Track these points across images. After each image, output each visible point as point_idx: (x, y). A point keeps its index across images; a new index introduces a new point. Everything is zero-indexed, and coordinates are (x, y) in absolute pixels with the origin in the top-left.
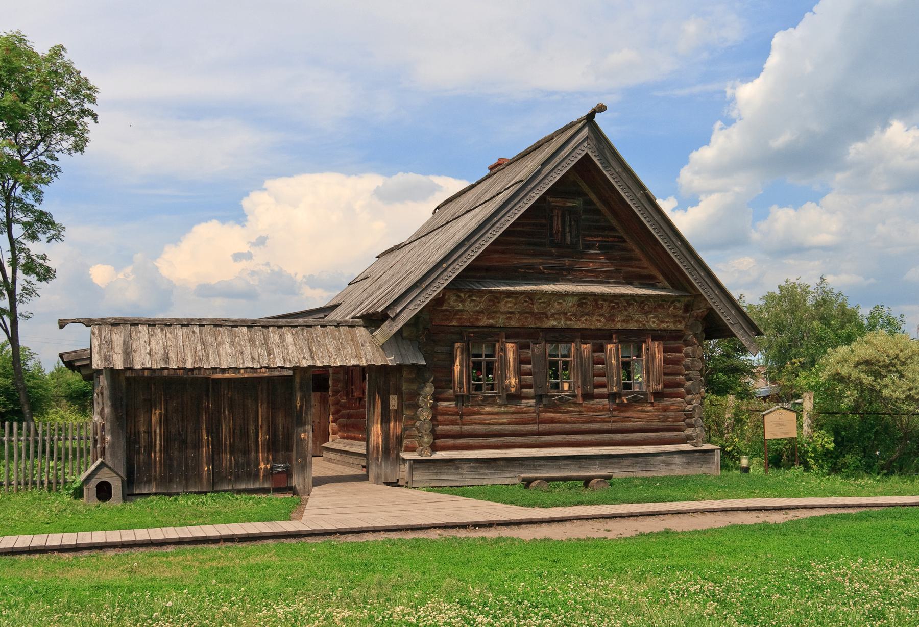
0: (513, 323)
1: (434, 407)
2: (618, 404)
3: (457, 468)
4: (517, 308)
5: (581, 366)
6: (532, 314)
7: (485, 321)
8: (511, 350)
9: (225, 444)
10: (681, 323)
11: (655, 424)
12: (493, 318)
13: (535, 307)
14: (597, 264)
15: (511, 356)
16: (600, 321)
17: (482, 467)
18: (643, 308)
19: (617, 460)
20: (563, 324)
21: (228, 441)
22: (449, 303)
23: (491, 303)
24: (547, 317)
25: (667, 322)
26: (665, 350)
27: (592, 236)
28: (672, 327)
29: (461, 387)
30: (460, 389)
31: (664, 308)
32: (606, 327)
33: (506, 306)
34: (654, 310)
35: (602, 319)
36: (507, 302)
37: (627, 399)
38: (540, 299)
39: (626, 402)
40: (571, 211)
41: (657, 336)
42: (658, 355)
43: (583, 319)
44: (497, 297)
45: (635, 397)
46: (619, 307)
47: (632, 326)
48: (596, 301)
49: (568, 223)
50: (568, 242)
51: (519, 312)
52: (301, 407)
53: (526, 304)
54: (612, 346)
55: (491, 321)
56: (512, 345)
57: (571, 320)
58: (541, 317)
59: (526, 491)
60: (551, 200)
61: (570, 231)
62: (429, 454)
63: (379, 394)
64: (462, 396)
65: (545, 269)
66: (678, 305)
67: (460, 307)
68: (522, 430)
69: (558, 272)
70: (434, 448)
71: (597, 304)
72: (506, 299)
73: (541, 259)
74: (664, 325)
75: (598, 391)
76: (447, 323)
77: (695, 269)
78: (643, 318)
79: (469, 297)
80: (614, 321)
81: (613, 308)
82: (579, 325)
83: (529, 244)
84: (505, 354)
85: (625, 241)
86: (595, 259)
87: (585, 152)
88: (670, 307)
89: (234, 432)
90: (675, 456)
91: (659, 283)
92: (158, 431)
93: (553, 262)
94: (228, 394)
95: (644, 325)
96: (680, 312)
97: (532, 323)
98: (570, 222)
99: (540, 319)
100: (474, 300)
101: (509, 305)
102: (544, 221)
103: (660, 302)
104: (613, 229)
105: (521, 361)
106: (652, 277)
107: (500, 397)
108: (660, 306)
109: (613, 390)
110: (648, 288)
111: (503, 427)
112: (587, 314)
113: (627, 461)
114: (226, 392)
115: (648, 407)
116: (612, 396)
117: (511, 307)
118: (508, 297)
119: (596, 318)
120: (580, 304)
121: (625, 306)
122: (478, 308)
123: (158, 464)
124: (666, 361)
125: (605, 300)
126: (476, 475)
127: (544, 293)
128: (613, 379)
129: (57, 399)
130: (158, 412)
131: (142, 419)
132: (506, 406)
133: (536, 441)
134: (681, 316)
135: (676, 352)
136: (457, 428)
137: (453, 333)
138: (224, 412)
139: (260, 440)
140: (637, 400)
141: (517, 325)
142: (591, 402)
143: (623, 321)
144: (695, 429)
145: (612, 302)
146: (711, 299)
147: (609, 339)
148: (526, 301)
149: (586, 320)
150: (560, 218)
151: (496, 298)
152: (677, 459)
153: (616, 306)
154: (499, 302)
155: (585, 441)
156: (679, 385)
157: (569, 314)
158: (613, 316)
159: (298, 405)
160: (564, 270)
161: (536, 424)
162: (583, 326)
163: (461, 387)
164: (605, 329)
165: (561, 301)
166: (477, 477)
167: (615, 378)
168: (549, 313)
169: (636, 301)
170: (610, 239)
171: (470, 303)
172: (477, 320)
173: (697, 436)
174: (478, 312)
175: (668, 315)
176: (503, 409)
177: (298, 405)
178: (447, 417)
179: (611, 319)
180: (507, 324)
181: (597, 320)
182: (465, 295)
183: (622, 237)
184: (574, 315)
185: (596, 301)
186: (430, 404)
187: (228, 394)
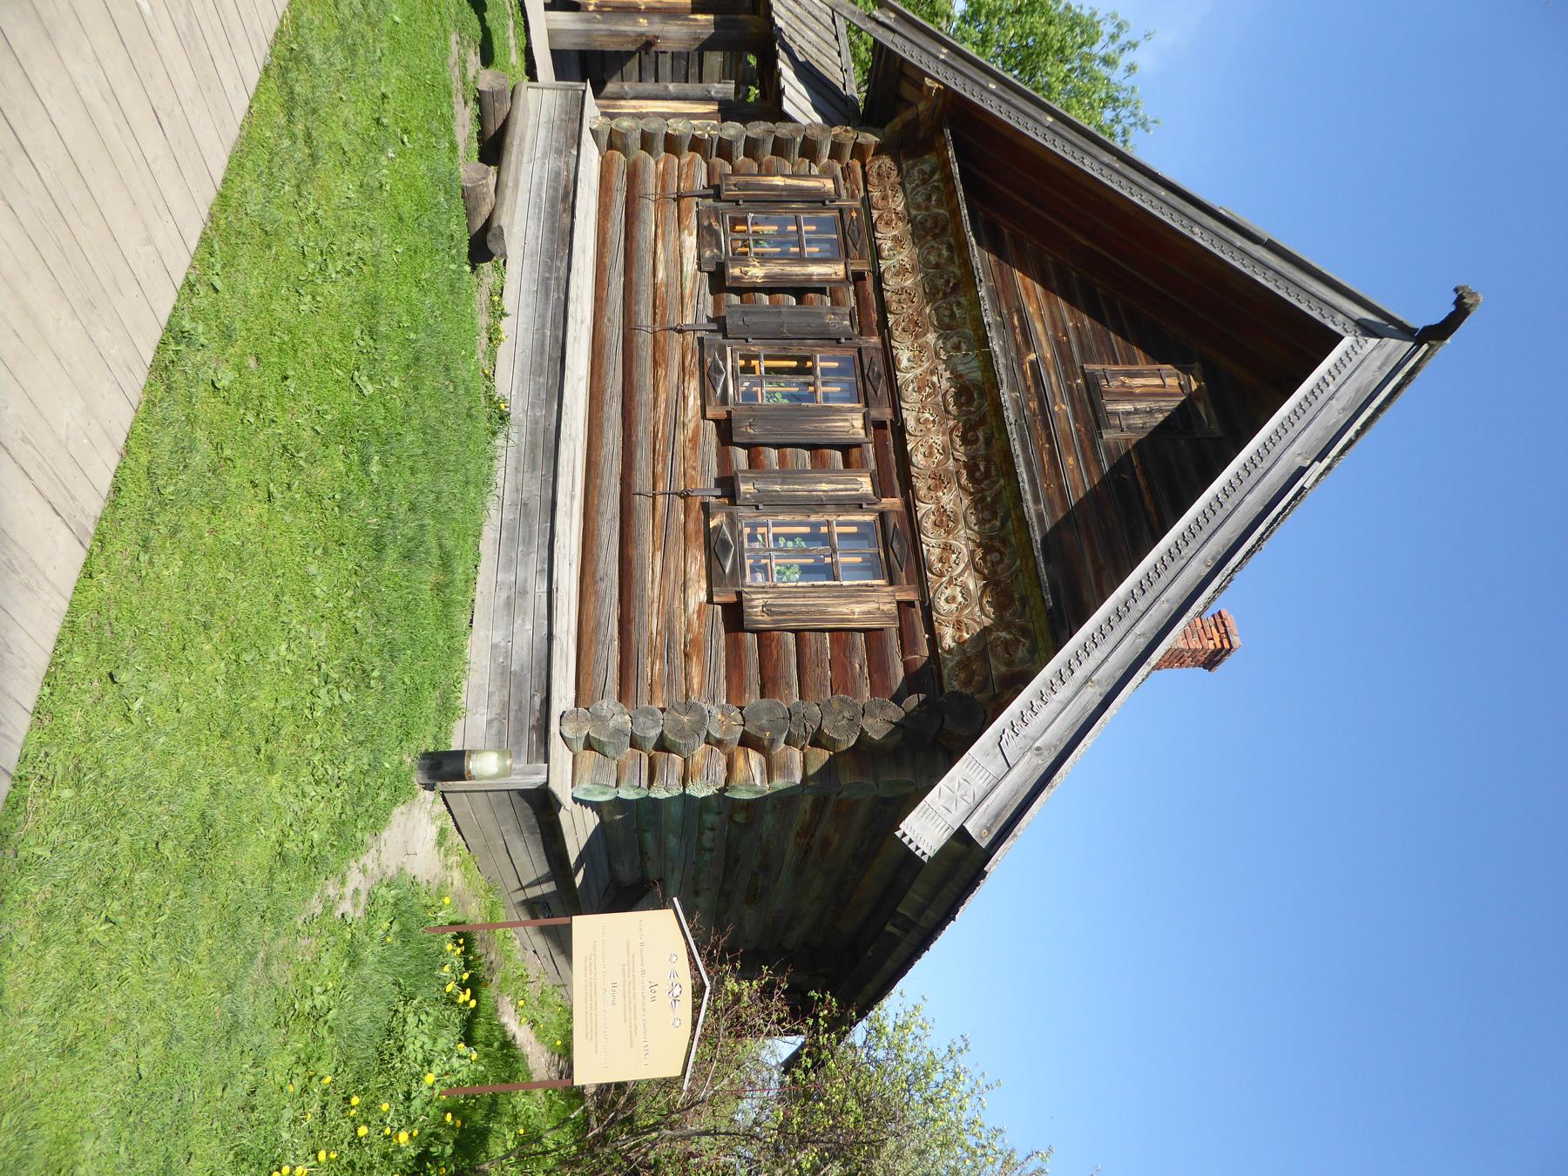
3: (559, 152)
14: (1077, 476)
17: (556, 190)
45: (726, 546)
47: (931, 543)
59: (491, 70)
65: (1032, 363)
68: (638, 303)
73: (1053, 356)
115: (698, 594)
118: (950, 248)
124: (841, 634)
126: (541, 178)
129: (684, 790)
148: (947, 282)
152: (526, 632)
154: (935, 237)
155: (601, 432)
167: (777, 488)
169: (1003, 524)
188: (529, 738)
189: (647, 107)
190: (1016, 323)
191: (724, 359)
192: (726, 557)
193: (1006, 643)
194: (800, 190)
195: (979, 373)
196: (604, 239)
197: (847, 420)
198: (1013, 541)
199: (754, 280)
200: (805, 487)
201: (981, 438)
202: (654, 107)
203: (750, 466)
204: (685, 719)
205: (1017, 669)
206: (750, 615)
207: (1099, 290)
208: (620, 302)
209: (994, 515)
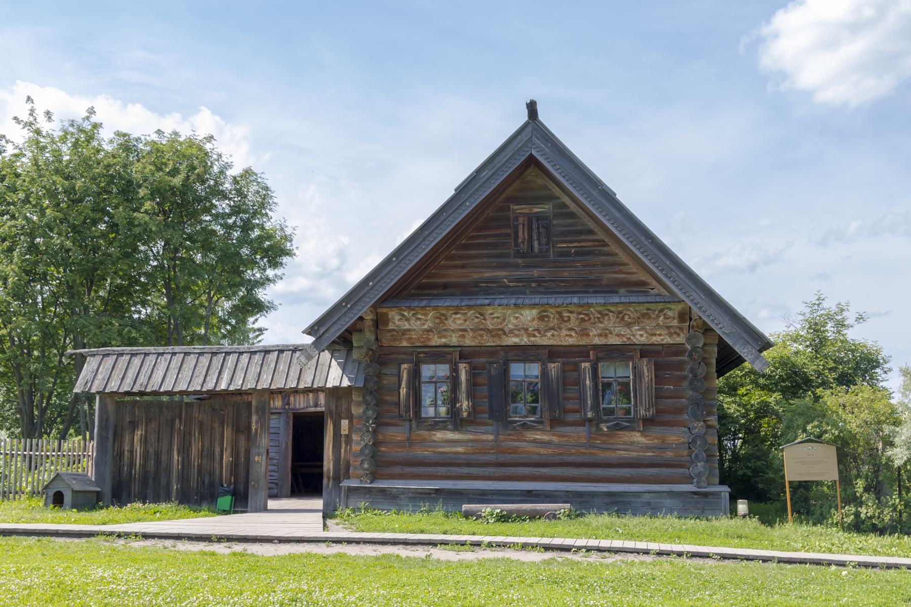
0: (468, 342)
6: (489, 331)
7: (436, 341)
9: (194, 464)
10: (679, 335)
12: (445, 337)
13: (488, 322)
16: (571, 336)
18: (623, 318)
20: (525, 340)
21: (197, 461)
22: (394, 323)
23: (438, 321)
24: (505, 334)
25: (660, 335)
27: (565, 242)
28: (668, 340)
30: (406, 413)
31: (650, 318)
32: (581, 343)
35: (573, 334)
36: (455, 319)
37: (608, 427)
39: (606, 430)
40: (539, 217)
43: (549, 334)
46: (590, 319)
47: (613, 340)
49: (535, 231)
50: (536, 250)
52: (256, 430)
53: (476, 320)
54: (587, 365)
55: (443, 340)
56: (465, 365)
57: (535, 336)
58: (498, 334)
60: (516, 207)
61: (538, 239)
62: (369, 481)
63: (331, 418)
66: (670, 313)
67: (407, 326)
69: (525, 284)
70: (374, 477)
71: (562, 317)
72: (454, 316)
74: (655, 339)
76: (397, 344)
78: (624, 331)
79: (414, 315)
80: (588, 335)
81: (583, 320)
82: (545, 341)
83: (491, 256)
85: (607, 245)
88: (658, 317)
89: (202, 453)
91: (652, 289)
93: (519, 273)
94: (198, 417)
95: (629, 339)
96: (675, 323)
98: (538, 229)
99: (499, 337)
100: (420, 319)
101: (459, 322)
102: (508, 231)
109: (587, 415)
112: (553, 329)
114: (197, 415)
117: (461, 325)
119: (564, 332)
122: (426, 327)
123: (137, 481)
130: (139, 433)
131: (127, 439)
133: (494, 473)
137: (404, 353)
138: (195, 434)
139: (224, 462)
141: (473, 344)
143: (600, 335)
148: (477, 317)
149: (553, 335)
150: (526, 226)
151: (443, 315)
153: (586, 318)
154: (446, 319)
157: (531, 329)
160: (534, 281)
162: (551, 342)
167: (589, 402)
168: (506, 329)
170: (590, 244)
172: (429, 339)
177: (253, 428)
180: (462, 344)
181: (567, 335)
182: (409, 313)
183: (603, 241)
184: (538, 330)
187: (198, 417)
189: (329, 456)
190: (484, 285)
191: (516, 422)
192: (622, 424)
194: (409, 381)
195: (534, 311)
196: (428, 476)
197: (551, 370)
198: (621, 309)
199: (470, 406)
200: (588, 390)
201: (568, 315)
202: (328, 452)
203: (579, 412)
204: (699, 443)
205: (676, 316)
206: (649, 416)
207: (463, 242)
208: (478, 469)
209: (607, 315)
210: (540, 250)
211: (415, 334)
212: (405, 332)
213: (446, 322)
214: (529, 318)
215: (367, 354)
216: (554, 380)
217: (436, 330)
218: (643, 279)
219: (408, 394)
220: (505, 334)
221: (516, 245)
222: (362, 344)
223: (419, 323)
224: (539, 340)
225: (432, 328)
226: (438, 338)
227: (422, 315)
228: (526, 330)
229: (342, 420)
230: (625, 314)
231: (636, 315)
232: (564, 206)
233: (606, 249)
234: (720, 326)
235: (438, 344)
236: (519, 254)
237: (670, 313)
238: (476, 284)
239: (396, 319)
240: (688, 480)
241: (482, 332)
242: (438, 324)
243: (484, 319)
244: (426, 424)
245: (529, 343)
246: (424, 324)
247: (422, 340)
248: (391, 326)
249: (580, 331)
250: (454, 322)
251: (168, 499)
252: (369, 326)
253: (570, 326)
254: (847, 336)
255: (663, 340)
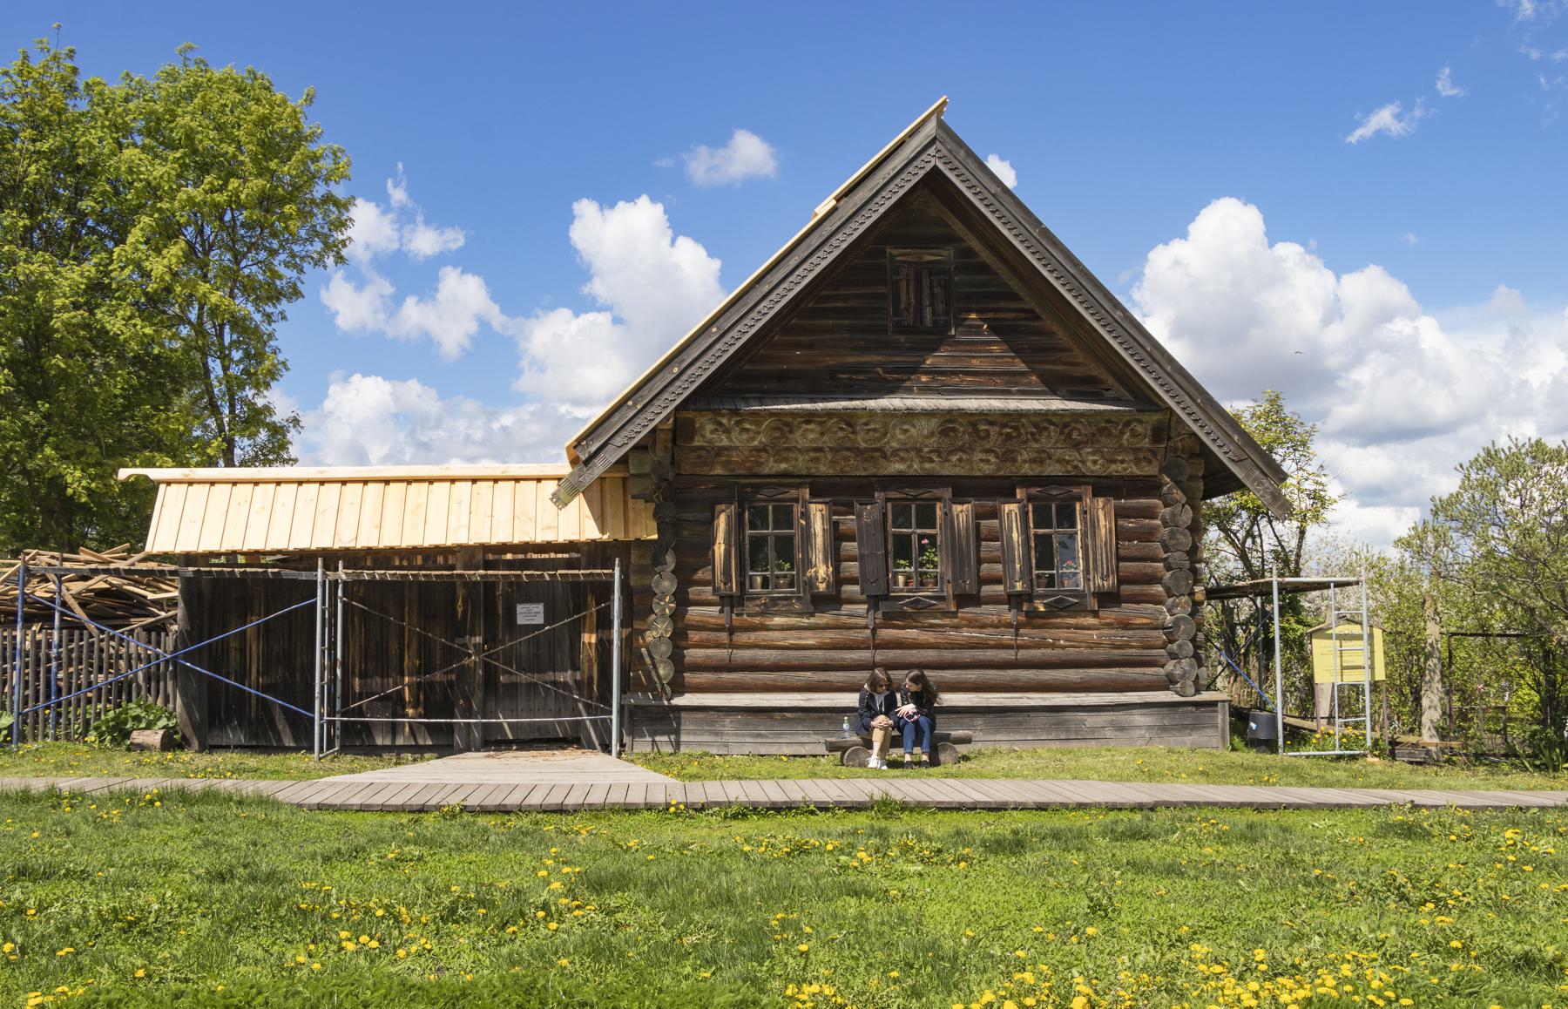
0: (823, 469)
1: (677, 616)
2: (1027, 614)
4: (828, 441)
5: (953, 545)
6: (858, 452)
7: (772, 466)
8: (819, 514)
10: (1150, 462)
11: (1101, 654)
12: (786, 460)
15: (818, 526)
16: (987, 461)
18: (1069, 436)
19: (1020, 717)
20: (916, 467)
22: (703, 436)
24: (885, 456)
25: (1122, 462)
26: (1120, 514)
29: (727, 580)
31: (1110, 434)
32: (1002, 473)
33: (807, 436)
34: (1091, 440)
36: (806, 430)
38: (866, 424)
40: (934, 269)
41: (1105, 486)
42: (1104, 524)
43: (954, 458)
44: (785, 423)
45: (1060, 601)
47: (1053, 469)
48: (974, 425)
49: (926, 291)
50: (928, 323)
51: (830, 448)
52: (465, 613)
53: (840, 434)
55: (783, 466)
56: (820, 506)
57: (931, 461)
58: (873, 458)
60: (895, 252)
61: (932, 305)
64: (731, 597)
66: (1139, 429)
67: (725, 442)
68: (844, 660)
71: (977, 431)
75: (987, 590)
76: (705, 470)
77: (1155, 360)
79: (738, 423)
80: (1015, 460)
81: (1009, 436)
82: (947, 470)
84: (809, 525)
85: (1037, 318)
86: (980, 352)
87: (932, 164)
88: (1122, 433)
90: (1134, 711)
92: (254, 648)
96: (1146, 443)
97: (857, 468)
98: (931, 288)
99: (873, 460)
100: (747, 430)
101: (811, 436)
102: (883, 290)
103: (1101, 428)
104: (1014, 297)
105: (837, 536)
106: (1094, 381)
107: (799, 598)
108: (1102, 431)
109: (1014, 587)
110: (1087, 401)
111: (808, 653)
112: (961, 449)
113: (1042, 718)
116: (1014, 600)
118: (808, 422)
120: (944, 433)
121: (1033, 434)
122: (756, 443)
124: (1121, 534)
125: (991, 423)
127: (871, 413)
128: (1014, 567)
132: (812, 615)
134: (1149, 450)
135: (1145, 518)
136: (721, 654)
140: (1061, 608)
141: (831, 472)
142: (977, 610)
143: (1033, 461)
144: (1179, 663)
145: (1005, 426)
146: (1190, 415)
147: (1010, 496)
148: (841, 429)
149: (960, 460)
151: (786, 424)
154: (791, 432)
156: (1153, 579)
157: (926, 450)
158: (1013, 451)
159: (460, 610)
161: (867, 648)
162: (958, 471)
163: (727, 580)
164: (999, 477)
165: (906, 427)
166: (748, 740)
167: (1018, 566)
170: (1012, 315)
171: (740, 433)
172: (759, 464)
173: (1183, 676)
174: (756, 449)
175: (1122, 449)
176: (805, 621)
177: (460, 610)
178: (704, 635)
179: (1008, 457)
180: (813, 471)
181: (981, 460)
182: (729, 420)
183: (1032, 311)
184: (938, 452)
185: (974, 425)
186: (670, 609)
188: (1203, 713)
193: (1132, 436)
205: (1149, 432)
209: (1046, 429)
210: (935, 322)
211: (738, 456)
212: (720, 451)
213: (791, 436)
214: (925, 432)
215: (658, 487)
216: (963, 532)
217: (773, 448)
218: (1094, 373)
219: (727, 553)
220: (885, 456)
221: (897, 312)
222: (647, 469)
223: (745, 436)
224: (936, 467)
225: (766, 445)
226: (776, 461)
227: (751, 424)
228: (919, 451)
229: (1502, 289)
230: (1074, 429)
231: (1090, 430)
232: (970, 252)
233: (1037, 324)
234: (1226, 449)
235: (773, 471)
236: (901, 329)
237: (1139, 429)
238: (833, 372)
239: (708, 432)
240: (1168, 683)
241: (848, 454)
242: (776, 438)
243: (853, 433)
244: (758, 602)
245: (920, 472)
246: (753, 439)
247: (748, 465)
248: (698, 442)
249: (1004, 454)
250: (804, 436)
251: (303, 742)
252: (666, 441)
253: (988, 446)
254: (278, 326)
255: (1125, 469)
